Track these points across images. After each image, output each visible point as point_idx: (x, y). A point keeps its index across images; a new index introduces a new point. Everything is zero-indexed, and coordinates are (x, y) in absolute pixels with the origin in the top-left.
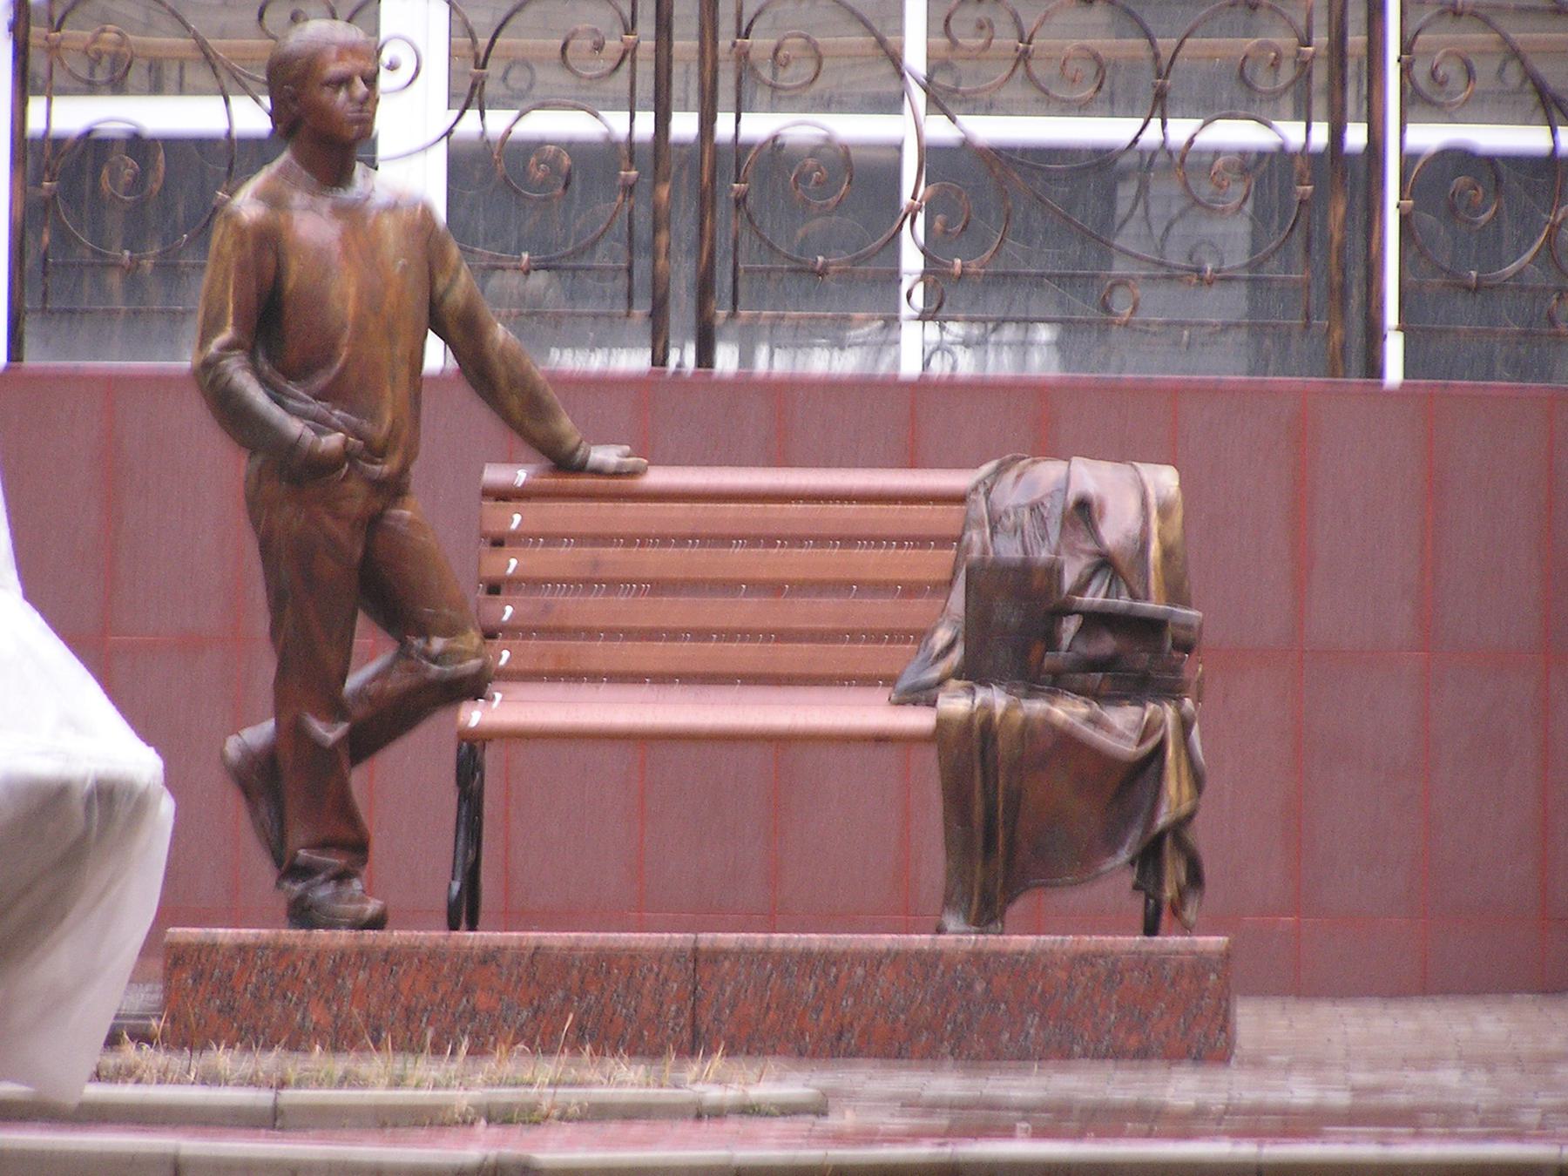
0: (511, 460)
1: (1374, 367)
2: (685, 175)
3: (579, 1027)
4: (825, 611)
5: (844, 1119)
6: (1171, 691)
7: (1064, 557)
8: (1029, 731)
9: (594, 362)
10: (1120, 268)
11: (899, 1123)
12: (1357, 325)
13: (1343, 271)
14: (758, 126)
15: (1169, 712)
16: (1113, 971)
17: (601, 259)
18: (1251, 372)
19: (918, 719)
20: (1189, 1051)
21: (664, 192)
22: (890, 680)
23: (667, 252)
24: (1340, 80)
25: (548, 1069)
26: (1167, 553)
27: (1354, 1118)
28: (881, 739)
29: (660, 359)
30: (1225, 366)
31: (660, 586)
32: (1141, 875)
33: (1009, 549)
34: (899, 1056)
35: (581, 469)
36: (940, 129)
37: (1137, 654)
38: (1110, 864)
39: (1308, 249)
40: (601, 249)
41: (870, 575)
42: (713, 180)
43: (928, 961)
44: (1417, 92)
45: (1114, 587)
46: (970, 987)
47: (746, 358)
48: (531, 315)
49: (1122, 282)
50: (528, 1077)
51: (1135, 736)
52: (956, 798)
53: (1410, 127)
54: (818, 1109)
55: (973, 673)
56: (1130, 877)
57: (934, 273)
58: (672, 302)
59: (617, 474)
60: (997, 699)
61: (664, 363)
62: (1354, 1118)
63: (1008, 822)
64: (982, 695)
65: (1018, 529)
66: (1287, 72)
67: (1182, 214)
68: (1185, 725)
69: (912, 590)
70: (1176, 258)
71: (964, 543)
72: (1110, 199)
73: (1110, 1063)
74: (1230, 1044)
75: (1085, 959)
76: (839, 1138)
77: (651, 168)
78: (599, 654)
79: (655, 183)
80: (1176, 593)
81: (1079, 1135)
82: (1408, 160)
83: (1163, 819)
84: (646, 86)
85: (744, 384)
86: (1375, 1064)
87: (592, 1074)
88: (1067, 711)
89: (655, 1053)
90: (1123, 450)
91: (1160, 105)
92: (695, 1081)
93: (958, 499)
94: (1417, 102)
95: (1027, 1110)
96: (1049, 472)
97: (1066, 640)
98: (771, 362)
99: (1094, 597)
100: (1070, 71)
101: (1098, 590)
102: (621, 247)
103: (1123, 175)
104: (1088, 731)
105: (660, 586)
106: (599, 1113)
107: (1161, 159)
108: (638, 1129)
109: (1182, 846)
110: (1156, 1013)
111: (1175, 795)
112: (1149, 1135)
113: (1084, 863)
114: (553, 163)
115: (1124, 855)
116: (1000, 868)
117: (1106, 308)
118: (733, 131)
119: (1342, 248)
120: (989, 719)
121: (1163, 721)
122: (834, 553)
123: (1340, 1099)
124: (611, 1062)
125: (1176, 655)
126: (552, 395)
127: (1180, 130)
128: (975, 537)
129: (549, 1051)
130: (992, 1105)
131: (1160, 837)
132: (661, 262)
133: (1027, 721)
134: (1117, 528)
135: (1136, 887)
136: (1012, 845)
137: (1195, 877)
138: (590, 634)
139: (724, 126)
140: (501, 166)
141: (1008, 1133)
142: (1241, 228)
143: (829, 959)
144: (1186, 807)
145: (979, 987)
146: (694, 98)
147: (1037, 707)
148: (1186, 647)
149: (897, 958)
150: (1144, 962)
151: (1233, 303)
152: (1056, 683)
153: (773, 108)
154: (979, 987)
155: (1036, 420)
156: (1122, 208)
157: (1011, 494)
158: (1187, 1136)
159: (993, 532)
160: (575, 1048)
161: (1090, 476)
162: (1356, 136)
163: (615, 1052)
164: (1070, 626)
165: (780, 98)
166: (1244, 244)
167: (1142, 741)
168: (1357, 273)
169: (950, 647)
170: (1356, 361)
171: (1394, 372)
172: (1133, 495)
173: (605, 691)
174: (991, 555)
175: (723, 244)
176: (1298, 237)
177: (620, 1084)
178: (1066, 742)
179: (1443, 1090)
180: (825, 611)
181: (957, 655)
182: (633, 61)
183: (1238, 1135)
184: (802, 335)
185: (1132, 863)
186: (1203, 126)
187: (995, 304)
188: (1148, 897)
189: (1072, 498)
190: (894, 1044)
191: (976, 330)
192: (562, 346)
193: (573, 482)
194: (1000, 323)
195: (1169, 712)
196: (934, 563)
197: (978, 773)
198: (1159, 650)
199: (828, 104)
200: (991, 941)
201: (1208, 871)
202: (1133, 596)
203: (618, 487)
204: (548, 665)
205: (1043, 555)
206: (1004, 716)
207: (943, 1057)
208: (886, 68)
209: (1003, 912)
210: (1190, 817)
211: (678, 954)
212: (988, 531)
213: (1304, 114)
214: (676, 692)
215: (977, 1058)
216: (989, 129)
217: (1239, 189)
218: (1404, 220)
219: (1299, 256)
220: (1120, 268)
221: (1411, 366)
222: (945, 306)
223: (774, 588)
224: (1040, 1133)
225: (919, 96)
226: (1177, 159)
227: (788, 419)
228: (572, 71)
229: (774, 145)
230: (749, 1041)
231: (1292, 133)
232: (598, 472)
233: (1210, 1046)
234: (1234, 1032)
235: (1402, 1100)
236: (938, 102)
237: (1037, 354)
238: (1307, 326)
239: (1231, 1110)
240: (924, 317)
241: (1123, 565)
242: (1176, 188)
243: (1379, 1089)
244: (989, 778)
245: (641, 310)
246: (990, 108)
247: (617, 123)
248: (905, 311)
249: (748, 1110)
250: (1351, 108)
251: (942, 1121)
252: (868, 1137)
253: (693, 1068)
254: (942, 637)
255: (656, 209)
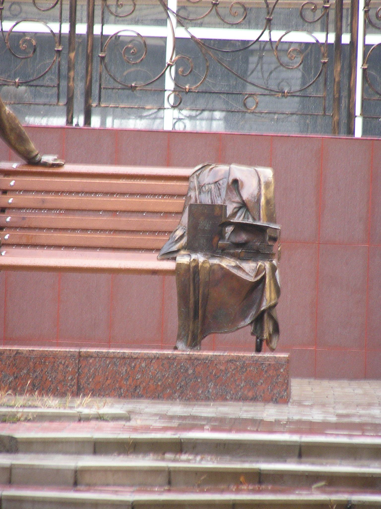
0: (10, 159)
1: (351, 131)
2: (80, 49)
3: (33, 385)
4: (133, 222)
5: (136, 422)
6: (268, 256)
7: (227, 203)
8: (212, 270)
9: (43, 121)
10: (250, 89)
11: (159, 424)
12: (344, 113)
13: (339, 92)
14: (110, 30)
15: (267, 265)
16: (243, 366)
17: (46, 81)
18: (301, 132)
19: (169, 265)
20: (272, 398)
21: (72, 55)
22: (158, 250)
23: (74, 78)
24: (339, 15)
25: (21, 400)
26: (268, 202)
27: (337, 426)
28: (154, 272)
29: (70, 121)
30: (291, 128)
31: (69, 211)
32: (255, 328)
33: (206, 199)
34: (158, 398)
35: (39, 163)
36: (182, 33)
37: (255, 240)
38: (242, 324)
39: (325, 84)
40: (47, 77)
41: (151, 208)
42: (92, 51)
43: (170, 360)
44: (370, 22)
45: (246, 216)
46: (187, 370)
47: (103, 122)
48: (19, 102)
49: (251, 95)
50: (12, 403)
51: (253, 274)
52: (183, 297)
53: (367, 37)
54: (127, 418)
55: (191, 247)
56: (250, 329)
57: (179, 90)
58: (75, 100)
59: (53, 165)
60: (200, 258)
61: (72, 122)
62: (337, 426)
63: (203, 307)
64: (194, 256)
65: (210, 191)
66: (319, 13)
67: (276, 68)
68: (273, 269)
69: (168, 214)
70: (273, 86)
71: (188, 196)
72: (247, 62)
73: (241, 403)
74: (289, 396)
75: (232, 361)
76: (135, 429)
77: (68, 46)
78: (44, 237)
79: (69, 52)
80: (271, 218)
81: (230, 431)
82: (366, 47)
83: (264, 306)
84: (66, 13)
85: (103, 131)
86: (347, 405)
87: (38, 403)
88: (227, 263)
89: (63, 395)
90: (251, 161)
91: (269, 24)
92: (79, 406)
93: (186, 179)
94: (370, 25)
95: (209, 420)
96: (223, 168)
97: (227, 236)
98: (112, 123)
99: (239, 219)
100: (234, 10)
101: (240, 216)
102: (55, 78)
103: (252, 52)
104: (235, 271)
105: (69, 211)
106: (41, 418)
107: (268, 46)
108: (55, 425)
109: (271, 317)
110: (259, 384)
111: (269, 297)
112: (257, 431)
113: (232, 322)
114: (29, 41)
115: (248, 321)
116: (200, 323)
117: (245, 105)
118: (104, 27)
119: (339, 83)
120: (197, 266)
121: (265, 269)
122: (137, 199)
123: (333, 419)
124: (45, 399)
125: (270, 243)
126: (27, 134)
127: (276, 35)
128: (192, 194)
129: (21, 394)
130: (194, 418)
131: (264, 311)
132: (71, 84)
133: (212, 266)
134: (248, 192)
135: (252, 334)
136: (204, 317)
137: (276, 329)
138: (41, 229)
139: (97, 30)
140: (8, 44)
141: (201, 428)
142: (298, 74)
143: (132, 358)
144: (273, 302)
145: (190, 372)
146: (85, 19)
147: (215, 261)
148: (274, 239)
149: (157, 358)
150: (256, 362)
151: (293, 104)
152: (223, 252)
153: (115, 23)
154: (190, 372)
155: (218, 148)
156: (251, 66)
157: (207, 177)
158: (271, 432)
159: (200, 193)
160: (31, 392)
161: (239, 171)
162: (346, 39)
163: (47, 394)
164: (229, 229)
165: (118, 21)
166: (299, 82)
167: (256, 276)
168: (344, 93)
169: (182, 237)
170: (343, 128)
171: (358, 133)
172: (255, 179)
173: (46, 251)
174: (198, 202)
175: (96, 76)
176: (321, 79)
177: (49, 407)
178: (227, 275)
179: (373, 417)
180: (133, 222)
181: (184, 241)
182: (61, 4)
183: (292, 432)
184: (126, 113)
185: (251, 323)
186: (286, 34)
187: (201, 102)
188: (257, 338)
189: (231, 180)
190: (157, 393)
191: (194, 113)
192: (31, 115)
193: (34, 169)
194: (203, 110)
195: (267, 265)
196: (176, 204)
197: (192, 289)
198: (264, 241)
199: (137, 22)
200: (195, 353)
201: (281, 328)
202: (254, 219)
203: (52, 170)
204: (24, 241)
205: (219, 202)
206: (202, 266)
207: (176, 399)
208: (161, 9)
209: (200, 342)
210: (275, 305)
211: (72, 355)
212: (197, 193)
213: (326, 29)
214: (74, 252)
215: (189, 399)
216: (201, 33)
217: (299, 59)
218: (364, 70)
219: (322, 86)
220: (250, 89)
221: (365, 131)
222: (181, 104)
223: (114, 212)
224: (214, 429)
225: (173, 19)
226: (274, 47)
227: (119, 145)
228: (37, 7)
229: (116, 37)
230: (100, 391)
231: (321, 37)
232: (45, 165)
233: (282, 398)
234: (290, 393)
235: (356, 420)
236: (181, 22)
237: (215, 122)
238: (325, 115)
239: (289, 422)
240: (173, 107)
241: (250, 205)
242: (274, 59)
243: (348, 416)
244: (196, 289)
245: (63, 101)
246: (201, 25)
247: (55, 27)
248: (166, 105)
249: (100, 418)
250: (344, 28)
251: (175, 423)
252: (147, 429)
253: (78, 401)
254: (179, 233)
255: (69, 62)
